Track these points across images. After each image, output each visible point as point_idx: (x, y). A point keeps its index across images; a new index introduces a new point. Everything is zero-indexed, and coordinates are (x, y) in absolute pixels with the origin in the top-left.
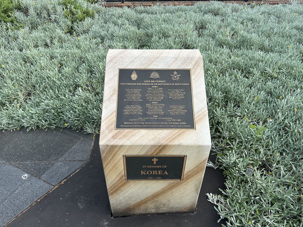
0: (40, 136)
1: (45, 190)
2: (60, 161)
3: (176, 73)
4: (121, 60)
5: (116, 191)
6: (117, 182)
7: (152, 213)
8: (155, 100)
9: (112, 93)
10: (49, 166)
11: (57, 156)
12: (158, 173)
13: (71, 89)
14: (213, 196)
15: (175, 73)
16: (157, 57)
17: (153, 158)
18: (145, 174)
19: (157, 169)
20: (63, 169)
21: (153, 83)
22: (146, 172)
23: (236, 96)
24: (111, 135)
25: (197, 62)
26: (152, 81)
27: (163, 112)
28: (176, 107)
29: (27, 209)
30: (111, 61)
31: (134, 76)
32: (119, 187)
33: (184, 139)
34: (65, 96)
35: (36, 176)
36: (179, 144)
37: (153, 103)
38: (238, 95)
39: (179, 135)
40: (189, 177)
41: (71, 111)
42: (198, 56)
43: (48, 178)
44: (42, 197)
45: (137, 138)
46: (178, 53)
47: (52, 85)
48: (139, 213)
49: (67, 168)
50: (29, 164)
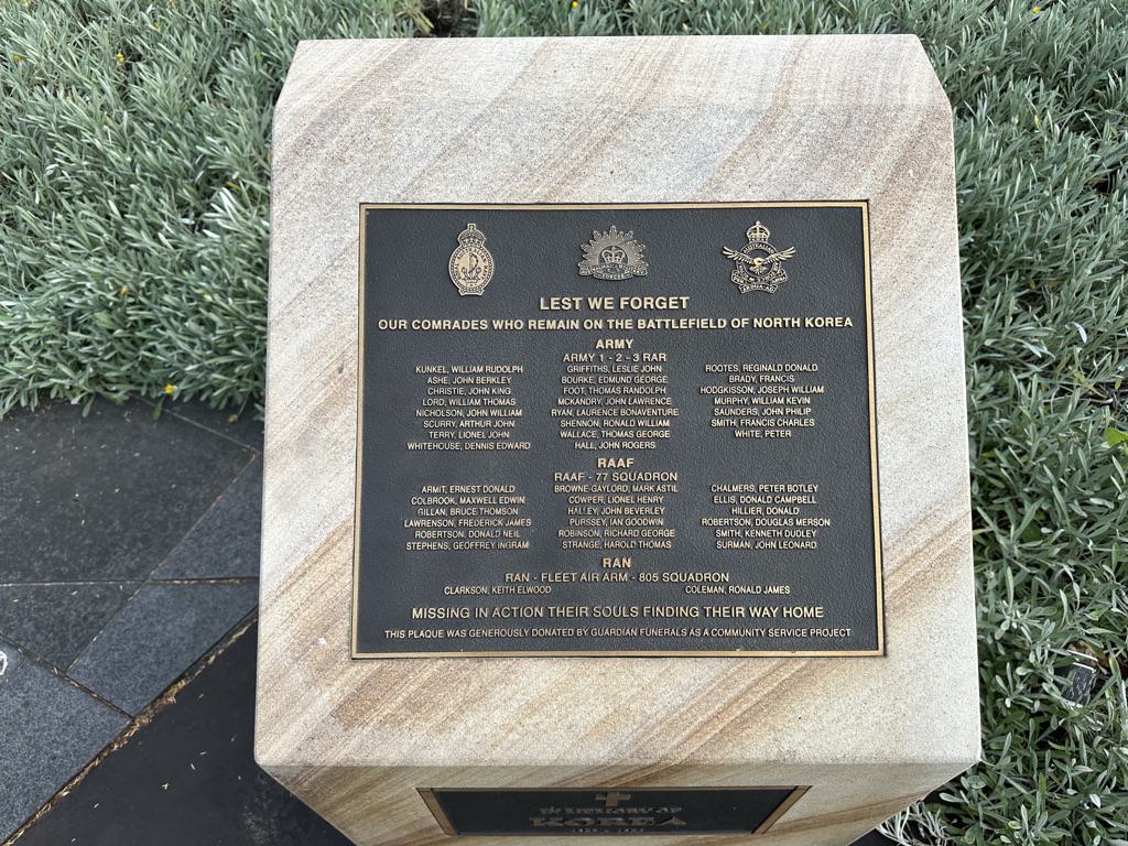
0: (61, 440)
1: (89, 742)
2: (155, 583)
3: (767, 234)
4: (375, 133)
8: (616, 445)
9: (320, 398)
10: (104, 609)
11: (139, 550)
13: (186, 194)
15: (759, 234)
16: (632, 113)
20: (170, 627)
21: (602, 313)
23: (1031, 243)
24: (326, 696)
25: (913, 144)
26: (594, 303)
27: (671, 533)
28: (757, 493)
29: (9, 838)
30: (306, 145)
31: (471, 266)
34: (154, 229)
35: (44, 665)
37: (602, 462)
38: (1040, 237)
39: (778, 694)
41: (191, 324)
42: (925, 99)
43: (100, 671)
44: (78, 775)
45: (498, 717)
46: (774, 72)
47: (88, 173)
49: (190, 619)
50: (14, 595)
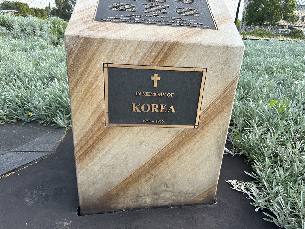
5: (87, 152)
6: (92, 127)
7: (146, 205)
12: (159, 109)
14: (238, 183)
17: (153, 72)
18: (138, 110)
19: (158, 101)
22: (141, 106)
32: (95, 141)
33: (203, 38)
36: (195, 42)
40: (209, 119)
48: (125, 206)
